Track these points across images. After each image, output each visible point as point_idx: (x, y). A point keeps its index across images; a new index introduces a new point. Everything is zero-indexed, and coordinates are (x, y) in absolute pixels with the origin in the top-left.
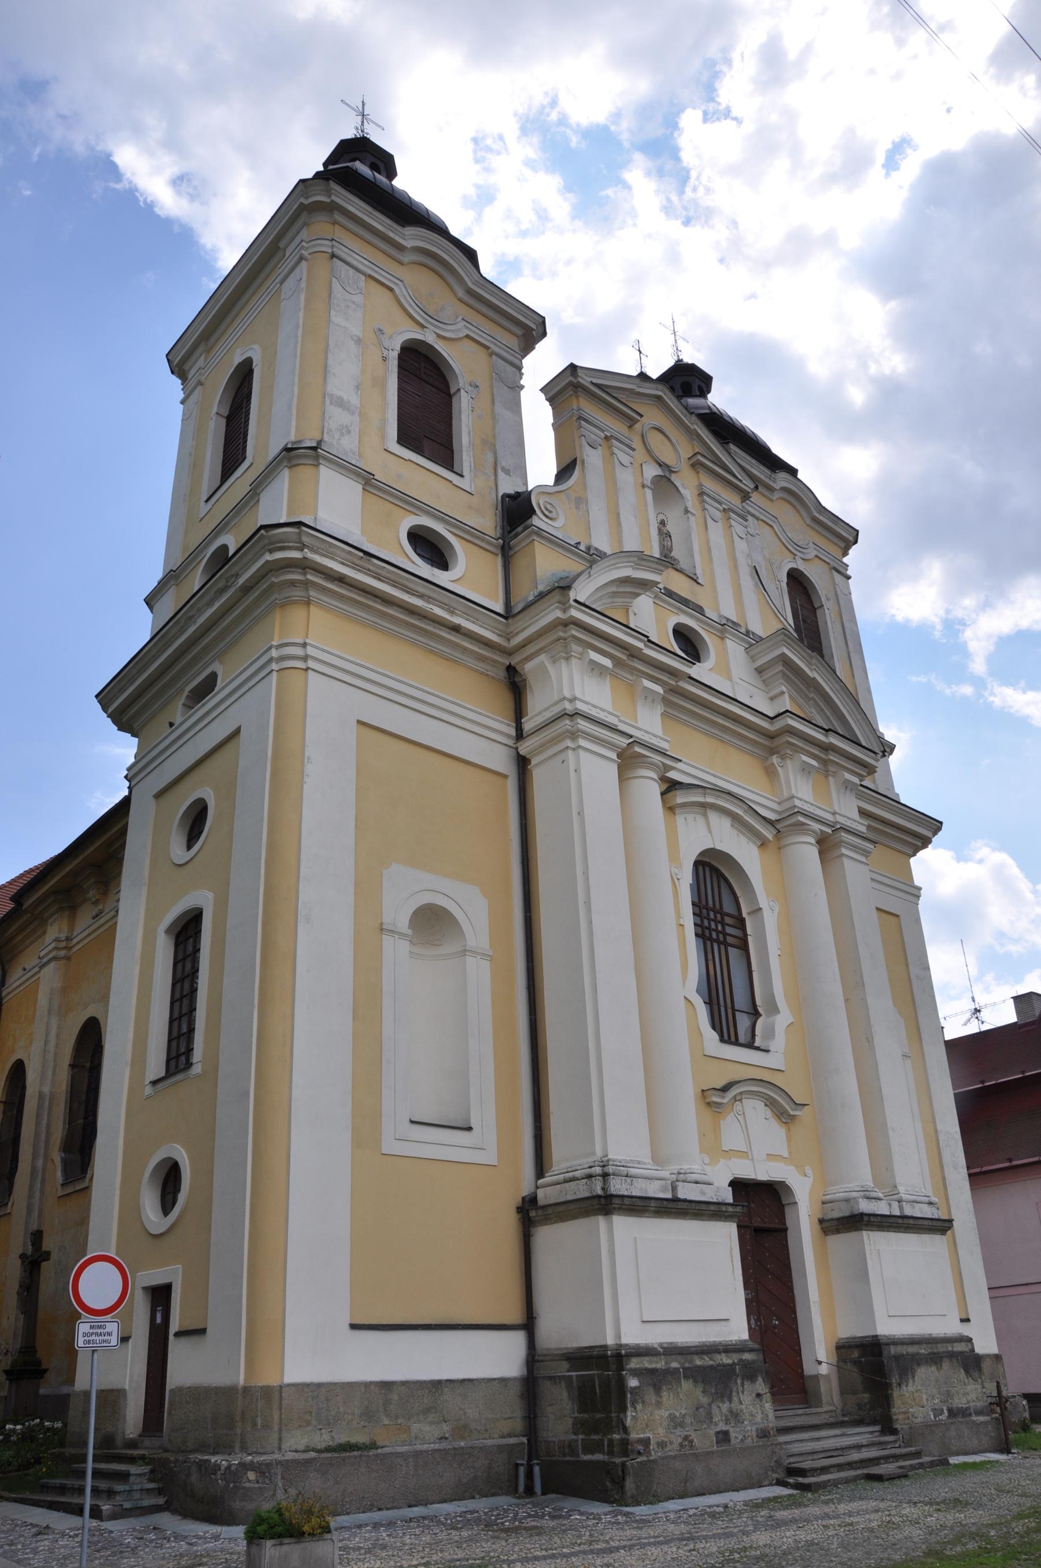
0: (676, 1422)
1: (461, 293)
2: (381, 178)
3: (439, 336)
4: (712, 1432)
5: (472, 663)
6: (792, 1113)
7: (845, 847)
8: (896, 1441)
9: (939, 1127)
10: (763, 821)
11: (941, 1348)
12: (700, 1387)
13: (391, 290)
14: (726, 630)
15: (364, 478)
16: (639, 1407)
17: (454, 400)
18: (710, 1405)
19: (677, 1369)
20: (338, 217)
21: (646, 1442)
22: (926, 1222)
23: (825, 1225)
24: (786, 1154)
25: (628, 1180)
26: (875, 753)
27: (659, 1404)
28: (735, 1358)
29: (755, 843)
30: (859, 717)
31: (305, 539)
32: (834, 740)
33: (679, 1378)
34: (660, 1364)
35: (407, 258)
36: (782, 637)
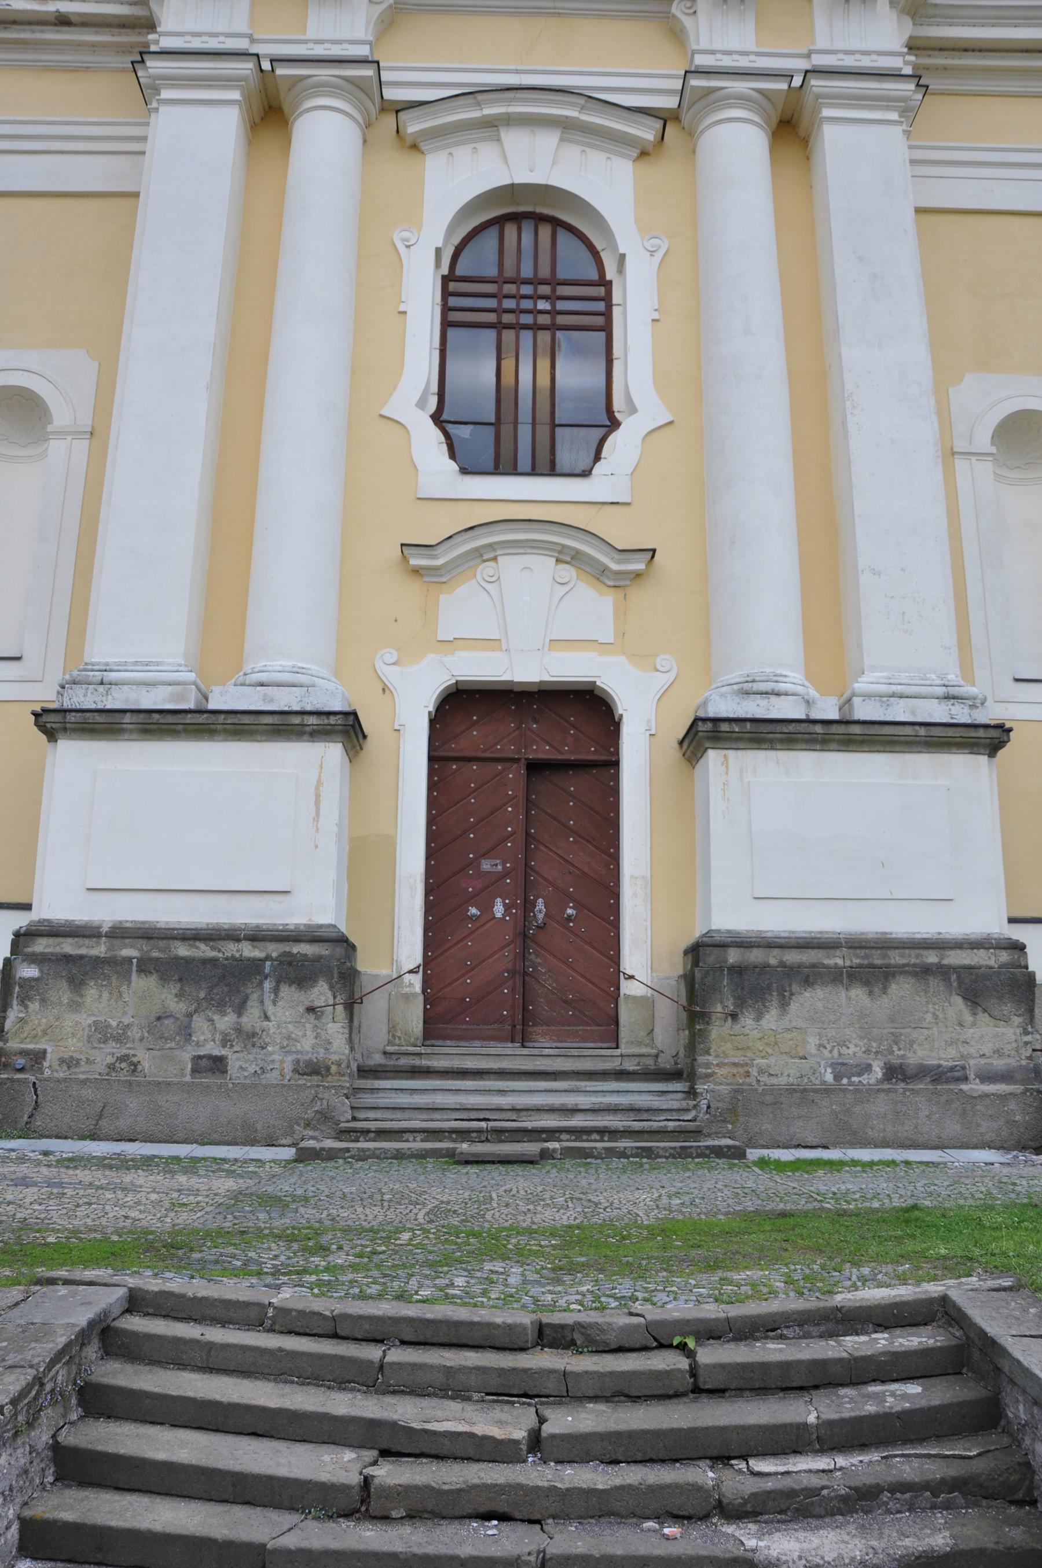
0: (102, 1033)
4: (186, 1056)
6: (615, 567)
8: (687, 1110)
11: (896, 958)
12: (174, 988)
16: (34, 1006)
18: (190, 1015)
19: (129, 960)
21: (39, 1056)
22: (908, 730)
23: (474, 736)
25: (101, 688)
27: (75, 1006)
28: (274, 950)
33: (130, 972)
34: (100, 949)
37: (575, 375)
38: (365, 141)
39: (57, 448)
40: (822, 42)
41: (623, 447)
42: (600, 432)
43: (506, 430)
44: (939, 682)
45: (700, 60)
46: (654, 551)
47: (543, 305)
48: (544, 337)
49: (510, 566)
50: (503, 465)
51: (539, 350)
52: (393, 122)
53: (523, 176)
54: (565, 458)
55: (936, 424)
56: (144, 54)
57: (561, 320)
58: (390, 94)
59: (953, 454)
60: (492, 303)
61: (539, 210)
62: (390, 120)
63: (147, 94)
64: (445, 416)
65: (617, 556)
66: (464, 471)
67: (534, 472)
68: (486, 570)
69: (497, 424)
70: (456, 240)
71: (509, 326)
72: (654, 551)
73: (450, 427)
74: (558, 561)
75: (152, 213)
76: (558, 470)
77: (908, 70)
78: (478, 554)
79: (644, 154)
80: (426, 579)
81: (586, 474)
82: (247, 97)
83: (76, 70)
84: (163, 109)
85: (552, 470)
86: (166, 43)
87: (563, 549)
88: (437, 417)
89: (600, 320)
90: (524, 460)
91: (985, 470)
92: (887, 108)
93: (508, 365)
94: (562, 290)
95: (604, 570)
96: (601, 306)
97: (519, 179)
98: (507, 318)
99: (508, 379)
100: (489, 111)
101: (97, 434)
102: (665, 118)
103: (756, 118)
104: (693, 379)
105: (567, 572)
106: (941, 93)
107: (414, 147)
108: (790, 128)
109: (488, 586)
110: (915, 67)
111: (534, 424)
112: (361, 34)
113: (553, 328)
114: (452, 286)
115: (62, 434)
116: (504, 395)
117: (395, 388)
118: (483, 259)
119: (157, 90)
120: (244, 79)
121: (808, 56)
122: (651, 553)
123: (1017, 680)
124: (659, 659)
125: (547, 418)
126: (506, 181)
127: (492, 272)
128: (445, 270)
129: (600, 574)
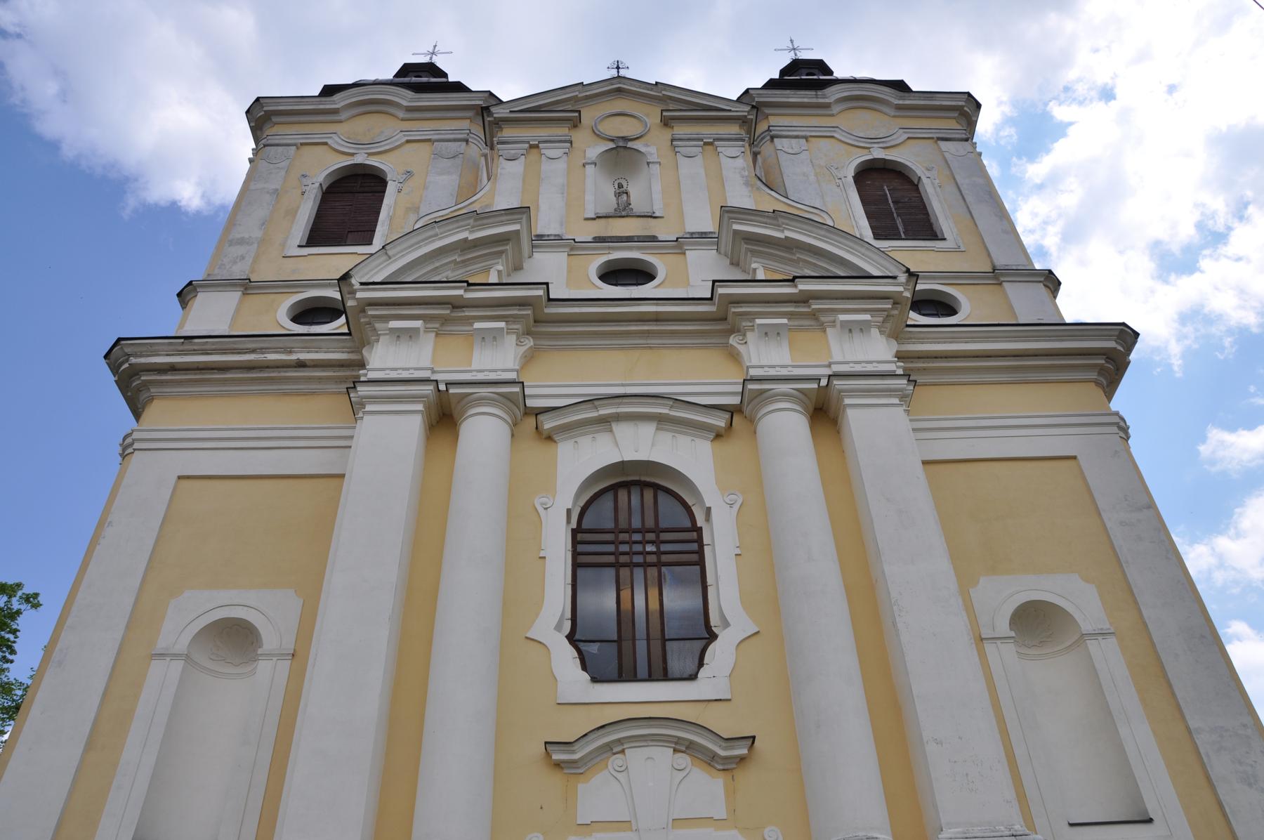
1: (401, 114)
2: (443, 80)
3: (369, 154)
5: (333, 387)
6: (723, 753)
7: (370, 403)
9: (1193, 724)
10: (703, 410)
13: (326, 144)
14: (683, 244)
15: (241, 285)
17: (920, 187)
20: (275, 119)
24: (721, 813)
26: (895, 278)
29: (706, 438)
30: (863, 250)
31: (127, 350)
32: (804, 286)
35: (343, 116)
36: (726, 215)
37: (678, 600)
38: (513, 435)
39: (264, 667)
40: (837, 357)
41: (720, 655)
42: (701, 644)
43: (626, 645)
44: (1008, 833)
45: (753, 372)
46: (754, 737)
47: (650, 548)
48: (652, 572)
49: (636, 757)
50: (626, 674)
51: (649, 582)
52: (533, 422)
53: (630, 456)
54: (674, 665)
55: (966, 618)
56: (356, 382)
57: (664, 558)
58: (530, 403)
59: (982, 639)
60: (611, 548)
61: (643, 479)
62: (531, 421)
63: (356, 409)
64: (577, 637)
65: (724, 744)
66: (595, 680)
67: (650, 678)
68: (616, 761)
69: (619, 641)
70: (582, 503)
71: (624, 565)
72: (754, 737)
73: (581, 645)
74: (675, 751)
75: (351, 487)
76: (670, 676)
77: (900, 372)
78: (608, 748)
79: (718, 436)
80: (566, 771)
81: (693, 677)
82: (428, 408)
83: (305, 394)
84: (366, 418)
85: (665, 676)
86: (372, 375)
87: (679, 740)
88: (571, 638)
89: (695, 557)
90: (642, 669)
91: (1009, 650)
92: (890, 396)
93: (625, 594)
94: (664, 536)
95: (714, 756)
96: (695, 546)
97: (629, 456)
98: (623, 559)
99: (626, 605)
100: (603, 412)
101: (298, 656)
102: (732, 411)
103: (798, 408)
104: (771, 596)
105: (684, 760)
106: (925, 385)
107: (549, 438)
108: (823, 412)
109: (619, 776)
110: (905, 369)
111: (648, 639)
112: (510, 365)
113: (659, 565)
114: (580, 537)
115: (269, 655)
116: (624, 617)
117: (537, 615)
118: (603, 516)
119: (363, 405)
120: (426, 396)
121: (829, 366)
122: (750, 742)
123: (1072, 825)
124: (766, 831)
125: (658, 635)
126: (616, 458)
127: (610, 525)
128: (574, 525)
129: (711, 760)
